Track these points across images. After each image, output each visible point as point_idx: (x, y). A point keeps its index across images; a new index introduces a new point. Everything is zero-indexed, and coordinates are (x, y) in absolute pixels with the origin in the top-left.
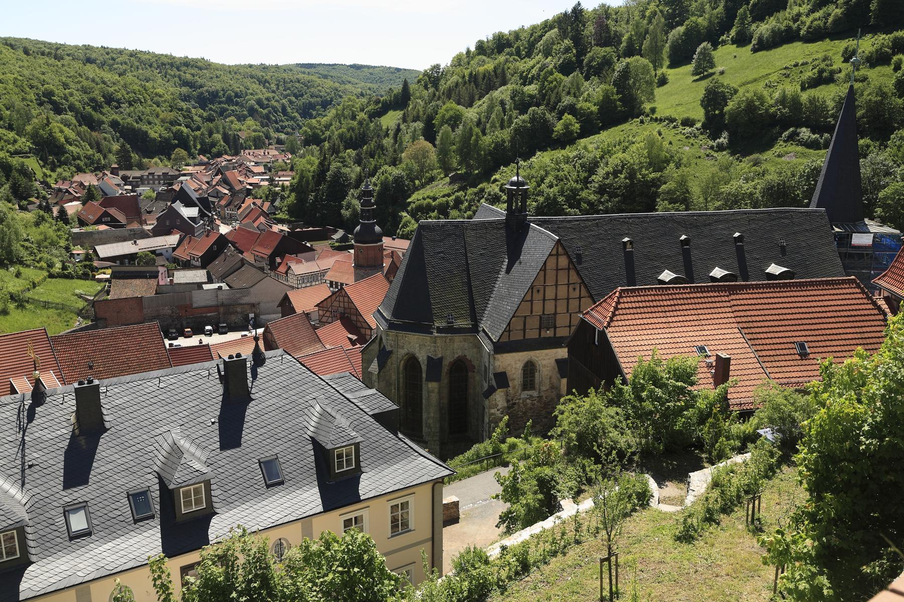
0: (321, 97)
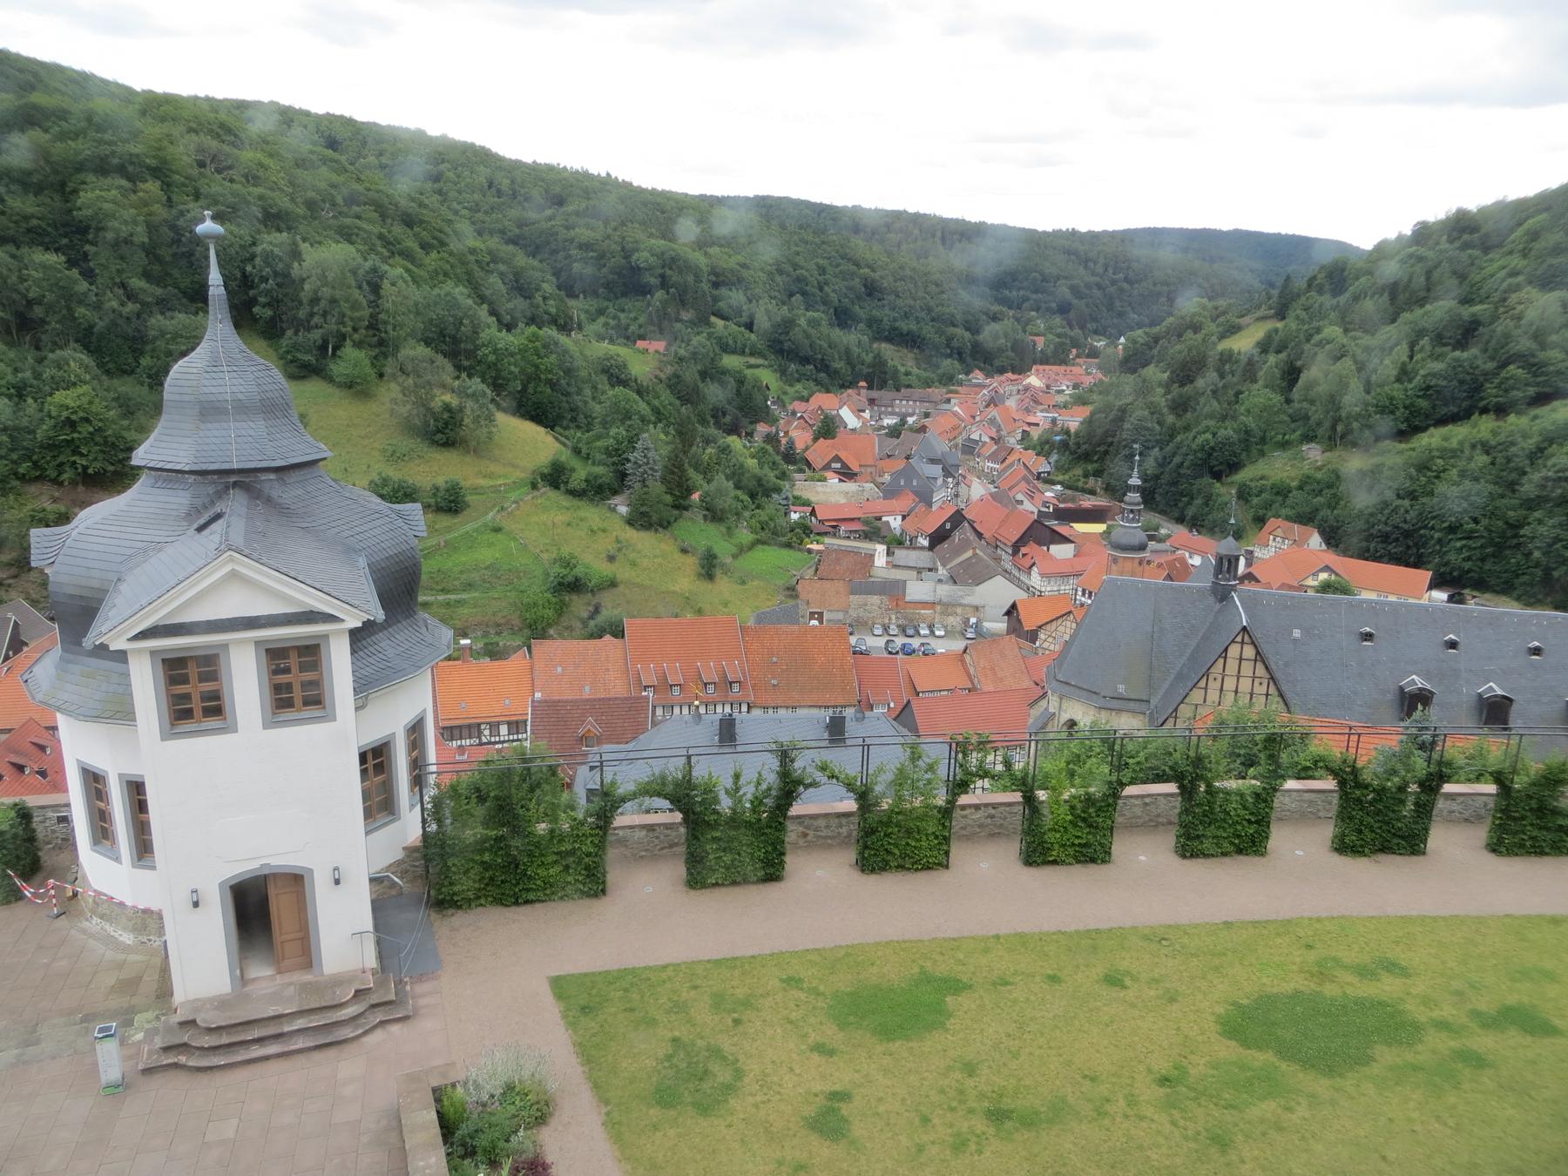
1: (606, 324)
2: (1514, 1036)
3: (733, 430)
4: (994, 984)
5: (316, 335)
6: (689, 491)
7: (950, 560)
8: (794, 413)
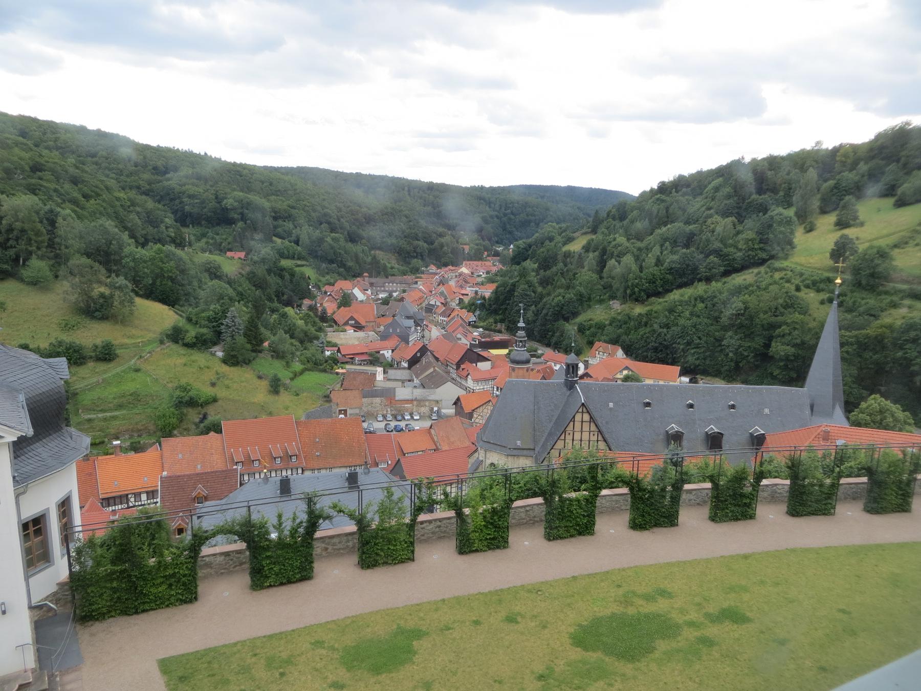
1: (207, 243)
2: (728, 626)
3: (289, 303)
4: (442, 630)
5: (12, 252)
6: (262, 341)
8: (326, 293)
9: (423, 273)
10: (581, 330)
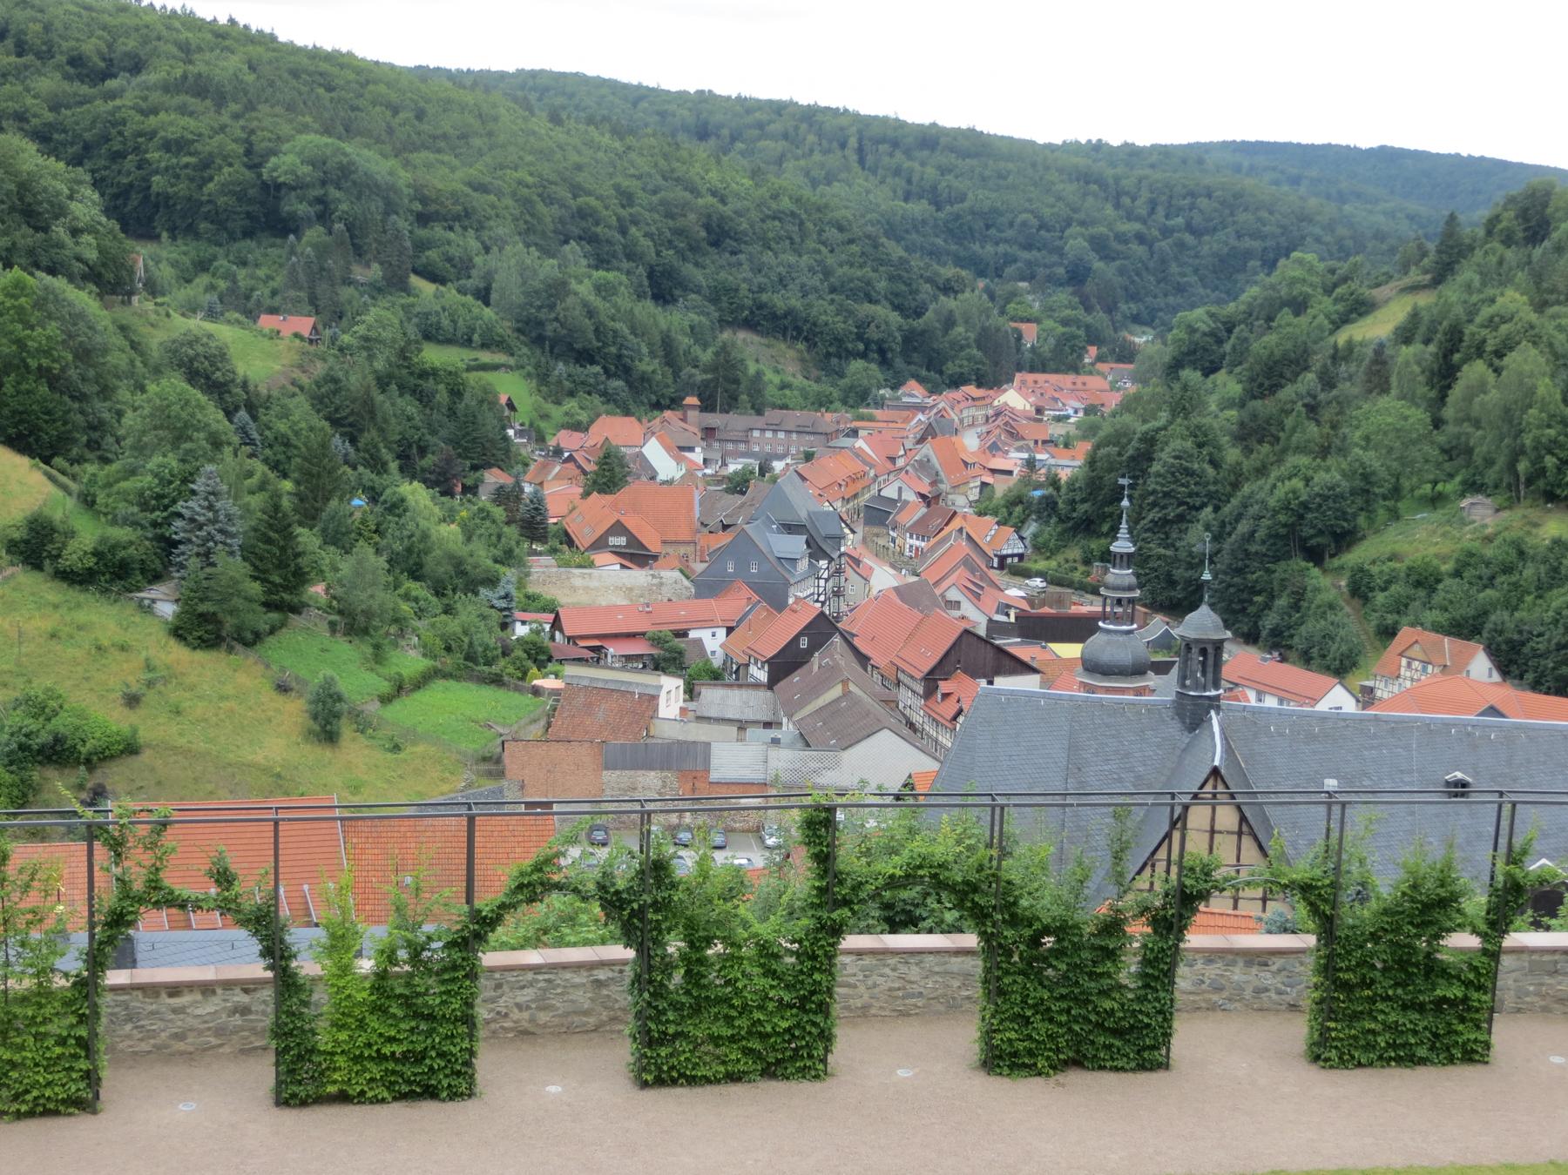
0: (1264, 238)
7: (802, 704)
9: (879, 403)
10: (1360, 589)
